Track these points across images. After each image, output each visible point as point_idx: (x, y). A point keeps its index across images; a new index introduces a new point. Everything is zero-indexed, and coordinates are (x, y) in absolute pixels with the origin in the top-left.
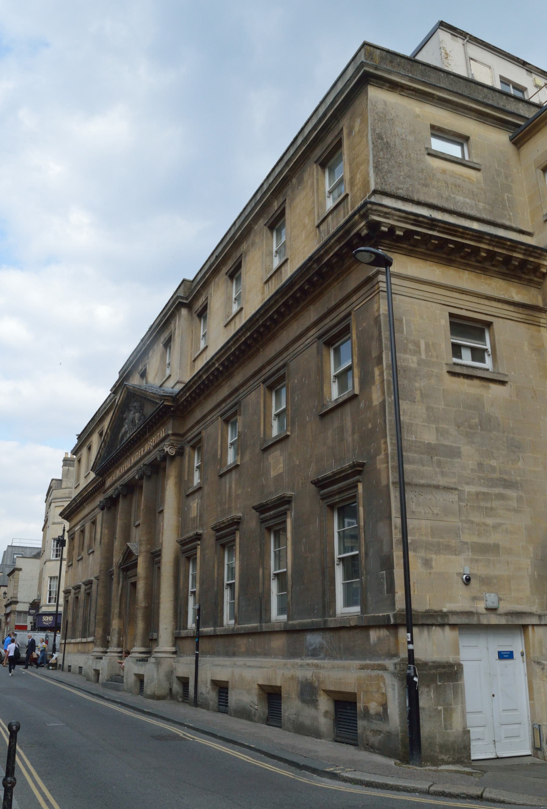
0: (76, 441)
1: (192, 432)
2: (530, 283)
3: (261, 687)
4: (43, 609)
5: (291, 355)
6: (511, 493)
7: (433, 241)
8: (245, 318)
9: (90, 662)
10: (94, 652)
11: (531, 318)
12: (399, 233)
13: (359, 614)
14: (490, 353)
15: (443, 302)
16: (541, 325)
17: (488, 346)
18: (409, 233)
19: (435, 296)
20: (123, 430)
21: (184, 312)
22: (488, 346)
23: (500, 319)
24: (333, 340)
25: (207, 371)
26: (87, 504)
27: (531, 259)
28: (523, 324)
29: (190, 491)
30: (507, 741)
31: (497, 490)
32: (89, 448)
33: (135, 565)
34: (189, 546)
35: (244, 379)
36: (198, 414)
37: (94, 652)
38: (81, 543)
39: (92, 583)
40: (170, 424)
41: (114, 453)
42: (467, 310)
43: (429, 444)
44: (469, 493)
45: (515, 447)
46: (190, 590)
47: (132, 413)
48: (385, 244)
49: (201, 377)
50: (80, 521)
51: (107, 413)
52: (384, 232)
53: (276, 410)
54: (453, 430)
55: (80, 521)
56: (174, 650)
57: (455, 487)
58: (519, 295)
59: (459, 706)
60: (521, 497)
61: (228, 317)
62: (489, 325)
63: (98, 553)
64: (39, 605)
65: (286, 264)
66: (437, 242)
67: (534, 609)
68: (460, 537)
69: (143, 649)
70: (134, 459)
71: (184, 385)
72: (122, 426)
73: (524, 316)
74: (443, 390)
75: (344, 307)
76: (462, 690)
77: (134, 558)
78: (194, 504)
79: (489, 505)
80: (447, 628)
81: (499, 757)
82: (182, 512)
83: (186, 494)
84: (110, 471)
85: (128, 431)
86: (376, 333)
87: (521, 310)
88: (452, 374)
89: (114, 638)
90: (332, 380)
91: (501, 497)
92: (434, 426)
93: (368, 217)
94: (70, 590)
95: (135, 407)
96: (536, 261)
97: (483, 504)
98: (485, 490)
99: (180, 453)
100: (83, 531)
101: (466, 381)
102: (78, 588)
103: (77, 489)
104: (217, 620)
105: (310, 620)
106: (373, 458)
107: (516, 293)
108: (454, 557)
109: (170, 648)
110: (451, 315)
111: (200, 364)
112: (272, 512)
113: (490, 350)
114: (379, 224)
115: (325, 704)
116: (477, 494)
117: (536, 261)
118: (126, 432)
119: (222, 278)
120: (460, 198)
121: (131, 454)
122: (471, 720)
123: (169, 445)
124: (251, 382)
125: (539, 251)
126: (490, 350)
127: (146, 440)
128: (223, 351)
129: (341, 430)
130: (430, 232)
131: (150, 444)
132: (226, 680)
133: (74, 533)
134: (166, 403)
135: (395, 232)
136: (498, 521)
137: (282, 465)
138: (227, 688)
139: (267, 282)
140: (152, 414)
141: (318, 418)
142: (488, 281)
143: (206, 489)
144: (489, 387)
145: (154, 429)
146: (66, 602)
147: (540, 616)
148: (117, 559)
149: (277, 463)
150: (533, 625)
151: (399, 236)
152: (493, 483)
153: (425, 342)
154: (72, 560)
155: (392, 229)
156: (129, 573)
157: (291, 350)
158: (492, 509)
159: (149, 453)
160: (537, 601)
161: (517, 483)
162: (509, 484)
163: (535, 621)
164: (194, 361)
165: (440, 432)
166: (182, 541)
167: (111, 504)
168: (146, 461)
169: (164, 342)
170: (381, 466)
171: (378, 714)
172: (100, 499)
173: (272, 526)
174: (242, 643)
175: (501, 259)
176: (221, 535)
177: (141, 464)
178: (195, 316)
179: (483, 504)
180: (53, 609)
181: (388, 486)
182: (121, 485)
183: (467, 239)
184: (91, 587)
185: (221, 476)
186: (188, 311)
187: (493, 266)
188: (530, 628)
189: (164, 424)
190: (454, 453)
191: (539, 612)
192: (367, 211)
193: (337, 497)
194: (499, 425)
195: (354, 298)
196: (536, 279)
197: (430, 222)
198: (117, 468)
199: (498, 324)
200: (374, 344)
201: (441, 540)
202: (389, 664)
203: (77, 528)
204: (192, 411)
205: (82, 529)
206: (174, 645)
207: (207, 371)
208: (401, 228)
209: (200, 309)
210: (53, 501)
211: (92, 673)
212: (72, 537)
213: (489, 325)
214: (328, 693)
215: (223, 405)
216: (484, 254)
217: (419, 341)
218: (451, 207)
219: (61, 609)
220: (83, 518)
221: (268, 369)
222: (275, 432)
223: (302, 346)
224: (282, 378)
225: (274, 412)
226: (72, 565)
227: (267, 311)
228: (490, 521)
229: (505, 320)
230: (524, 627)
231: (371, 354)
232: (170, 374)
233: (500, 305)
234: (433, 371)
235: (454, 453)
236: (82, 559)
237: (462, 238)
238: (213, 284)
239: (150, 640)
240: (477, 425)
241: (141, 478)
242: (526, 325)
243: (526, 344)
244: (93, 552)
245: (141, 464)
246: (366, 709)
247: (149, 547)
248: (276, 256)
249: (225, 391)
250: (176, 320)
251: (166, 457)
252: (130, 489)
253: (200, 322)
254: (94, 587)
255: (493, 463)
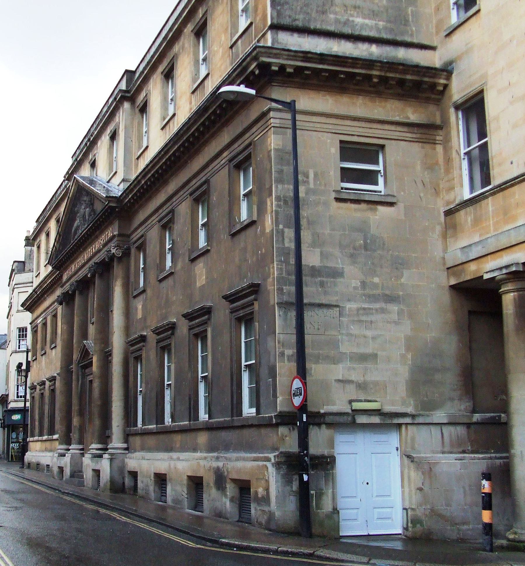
0: (35, 224)
1: (136, 233)
2: (428, 100)
3: (189, 477)
4: (12, 405)
5: (211, 172)
6: (394, 308)
7: (323, 74)
8: (177, 124)
9: (55, 459)
10: (58, 449)
11: (428, 136)
12: (289, 70)
13: (255, 415)
14: (382, 174)
15: (334, 132)
16: (437, 142)
17: (380, 168)
18: (299, 70)
19: (326, 126)
20: (75, 225)
21: (127, 105)
22: (380, 168)
23: (393, 141)
24: (241, 164)
25: (144, 177)
26: (47, 296)
27: (426, 79)
28: (417, 144)
29: (238, 227)
30: (379, 521)
31: (377, 306)
32: (48, 235)
33: (91, 364)
34: (136, 347)
35: (178, 187)
36: (141, 216)
37: (58, 449)
38: (44, 338)
39: (55, 380)
40: (116, 225)
41: (68, 248)
42: (358, 136)
43: (313, 267)
44: (350, 309)
45: (399, 265)
46: (166, 383)
47: (83, 207)
48: (278, 80)
49: (139, 182)
50: (42, 313)
51: (62, 200)
52: (274, 71)
53: (244, 190)
54: (337, 252)
55: (42, 313)
56: (126, 447)
57: (337, 304)
58: (415, 115)
59: (330, 491)
60: (402, 310)
61: (164, 119)
62: (383, 147)
63: (59, 348)
64: (7, 401)
65: (207, 79)
66: (327, 74)
67: (410, 410)
68: (338, 347)
69: (100, 446)
70: (86, 255)
71: (129, 184)
72: (75, 220)
73: (418, 136)
74: (330, 217)
75: (247, 135)
76: (333, 478)
77: (91, 357)
78: (139, 305)
79: (369, 319)
80: (324, 427)
81: (370, 534)
82: (128, 312)
83: (129, 296)
84: (66, 265)
85: (80, 226)
86: (268, 167)
87: (415, 130)
88: (338, 200)
89: (75, 435)
90: (241, 199)
91: (383, 311)
92: (319, 250)
93: (259, 58)
94: (36, 386)
95: (85, 201)
96: (431, 80)
97: (364, 318)
98: (366, 306)
99: (127, 254)
100: (45, 324)
101: (353, 206)
102: (43, 383)
103: (38, 278)
104: (160, 419)
105: (223, 419)
106: (265, 279)
107: (413, 114)
108: (333, 366)
109: (122, 444)
110: (341, 142)
111: (143, 164)
112: (197, 321)
113: (382, 171)
114: (269, 64)
115: (231, 490)
116: (358, 310)
117: (431, 80)
118: (78, 227)
119: (187, 39)
120: (359, 20)
121: (85, 249)
122: (341, 504)
123: (115, 247)
124: (182, 193)
125: (434, 71)
126: (382, 171)
127: (97, 237)
128: (158, 158)
129: (245, 249)
130: (321, 66)
131: (97, 245)
132: (163, 472)
133: (37, 326)
134: (112, 204)
135: (285, 69)
136: (376, 333)
137: (204, 277)
138: (166, 480)
139: (193, 92)
140: (102, 211)
141: (230, 237)
142: (383, 104)
143: (149, 291)
144: (376, 210)
145: (103, 227)
146: (33, 398)
147: (413, 416)
148: (76, 356)
149: (201, 273)
150: (407, 424)
151: (290, 73)
152: (374, 298)
153: (314, 172)
154: (36, 354)
155: (282, 67)
156: (87, 371)
157: (210, 168)
158: (371, 322)
159: (99, 251)
160: (412, 402)
161: (399, 297)
162: (390, 299)
163: (408, 420)
164: (138, 159)
165: (324, 256)
166: (129, 342)
167: (67, 299)
168: (96, 259)
169: (111, 135)
170: (270, 288)
171: (263, 497)
172: (59, 292)
173: (243, 316)
174: (178, 438)
175: (394, 83)
176: (161, 338)
177: (91, 262)
178: (137, 110)
179: (364, 318)
180: (21, 405)
181: (274, 306)
182: (77, 281)
183: (357, 68)
184: (55, 383)
185: (234, 235)
186: (131, 104)
187: (388, 89)
188: (404, 427)
189: (111, 223)
190: (336, 274)
191: (414, 412)
192: (257, 54)
193: (241, 311)
194: (384, 244)
195: (254, 129)
196: (433, 96)
197: (319, 57)
198: (72, 262)
199: (390, 146)
200: (267, 176)
201: (321, 352)
202: (271, 456)
203: (39, 320)
204: (136, 212)
205: (44, 321)
206: (126, 441)
207: (144, 177)
208: (291, 66)
209: (142, 104)
210: (16, 286)
211: (55, 470)
212: (34, 330)
213: (383, 147)
214: (234, 481)
215: (161, 211)
216: (375, 80)
217: (308, 172)
218: (347, 30)
219: (28, 404)
220: (45, 311)
221: (194, 182)
222: (244, 216)
223: (219, 165)
224: (248, 158)
225: (242, 192)
226: (36, 359)
227: (189, 129)
228: (369, 333)
229: (398, 141)
230: (399, 426)
231: (265, 185)
232: (112, 174)
233: (393, 128)
234: (320, 199)
235: (336, 274)
236: (45, 353)
237: (353, 67)
238: (152, 80)
239: (105, 438)
240: (367, 247)
241: (93, 276)
242: (420, 144)
243: (419, 162)
244: (55, 347)
245: (91, 262)
246: (256, 493)
247: (103, 345)
248: (202, 64)
249: (161, 198)
250: (119, 113)
251: (112, 258)
252: (84, 285)
253: (168, 83)
254: (58, 384)
255: (376, 280)
